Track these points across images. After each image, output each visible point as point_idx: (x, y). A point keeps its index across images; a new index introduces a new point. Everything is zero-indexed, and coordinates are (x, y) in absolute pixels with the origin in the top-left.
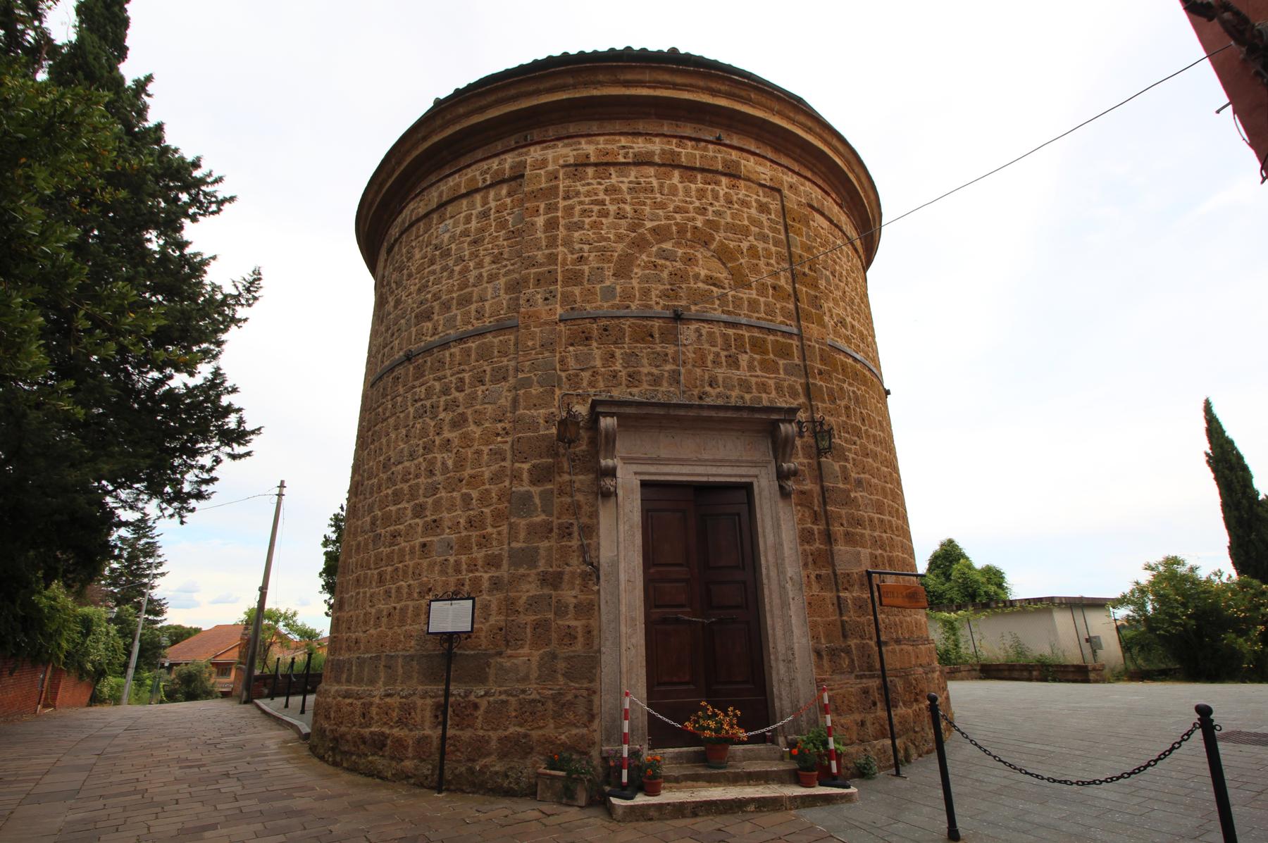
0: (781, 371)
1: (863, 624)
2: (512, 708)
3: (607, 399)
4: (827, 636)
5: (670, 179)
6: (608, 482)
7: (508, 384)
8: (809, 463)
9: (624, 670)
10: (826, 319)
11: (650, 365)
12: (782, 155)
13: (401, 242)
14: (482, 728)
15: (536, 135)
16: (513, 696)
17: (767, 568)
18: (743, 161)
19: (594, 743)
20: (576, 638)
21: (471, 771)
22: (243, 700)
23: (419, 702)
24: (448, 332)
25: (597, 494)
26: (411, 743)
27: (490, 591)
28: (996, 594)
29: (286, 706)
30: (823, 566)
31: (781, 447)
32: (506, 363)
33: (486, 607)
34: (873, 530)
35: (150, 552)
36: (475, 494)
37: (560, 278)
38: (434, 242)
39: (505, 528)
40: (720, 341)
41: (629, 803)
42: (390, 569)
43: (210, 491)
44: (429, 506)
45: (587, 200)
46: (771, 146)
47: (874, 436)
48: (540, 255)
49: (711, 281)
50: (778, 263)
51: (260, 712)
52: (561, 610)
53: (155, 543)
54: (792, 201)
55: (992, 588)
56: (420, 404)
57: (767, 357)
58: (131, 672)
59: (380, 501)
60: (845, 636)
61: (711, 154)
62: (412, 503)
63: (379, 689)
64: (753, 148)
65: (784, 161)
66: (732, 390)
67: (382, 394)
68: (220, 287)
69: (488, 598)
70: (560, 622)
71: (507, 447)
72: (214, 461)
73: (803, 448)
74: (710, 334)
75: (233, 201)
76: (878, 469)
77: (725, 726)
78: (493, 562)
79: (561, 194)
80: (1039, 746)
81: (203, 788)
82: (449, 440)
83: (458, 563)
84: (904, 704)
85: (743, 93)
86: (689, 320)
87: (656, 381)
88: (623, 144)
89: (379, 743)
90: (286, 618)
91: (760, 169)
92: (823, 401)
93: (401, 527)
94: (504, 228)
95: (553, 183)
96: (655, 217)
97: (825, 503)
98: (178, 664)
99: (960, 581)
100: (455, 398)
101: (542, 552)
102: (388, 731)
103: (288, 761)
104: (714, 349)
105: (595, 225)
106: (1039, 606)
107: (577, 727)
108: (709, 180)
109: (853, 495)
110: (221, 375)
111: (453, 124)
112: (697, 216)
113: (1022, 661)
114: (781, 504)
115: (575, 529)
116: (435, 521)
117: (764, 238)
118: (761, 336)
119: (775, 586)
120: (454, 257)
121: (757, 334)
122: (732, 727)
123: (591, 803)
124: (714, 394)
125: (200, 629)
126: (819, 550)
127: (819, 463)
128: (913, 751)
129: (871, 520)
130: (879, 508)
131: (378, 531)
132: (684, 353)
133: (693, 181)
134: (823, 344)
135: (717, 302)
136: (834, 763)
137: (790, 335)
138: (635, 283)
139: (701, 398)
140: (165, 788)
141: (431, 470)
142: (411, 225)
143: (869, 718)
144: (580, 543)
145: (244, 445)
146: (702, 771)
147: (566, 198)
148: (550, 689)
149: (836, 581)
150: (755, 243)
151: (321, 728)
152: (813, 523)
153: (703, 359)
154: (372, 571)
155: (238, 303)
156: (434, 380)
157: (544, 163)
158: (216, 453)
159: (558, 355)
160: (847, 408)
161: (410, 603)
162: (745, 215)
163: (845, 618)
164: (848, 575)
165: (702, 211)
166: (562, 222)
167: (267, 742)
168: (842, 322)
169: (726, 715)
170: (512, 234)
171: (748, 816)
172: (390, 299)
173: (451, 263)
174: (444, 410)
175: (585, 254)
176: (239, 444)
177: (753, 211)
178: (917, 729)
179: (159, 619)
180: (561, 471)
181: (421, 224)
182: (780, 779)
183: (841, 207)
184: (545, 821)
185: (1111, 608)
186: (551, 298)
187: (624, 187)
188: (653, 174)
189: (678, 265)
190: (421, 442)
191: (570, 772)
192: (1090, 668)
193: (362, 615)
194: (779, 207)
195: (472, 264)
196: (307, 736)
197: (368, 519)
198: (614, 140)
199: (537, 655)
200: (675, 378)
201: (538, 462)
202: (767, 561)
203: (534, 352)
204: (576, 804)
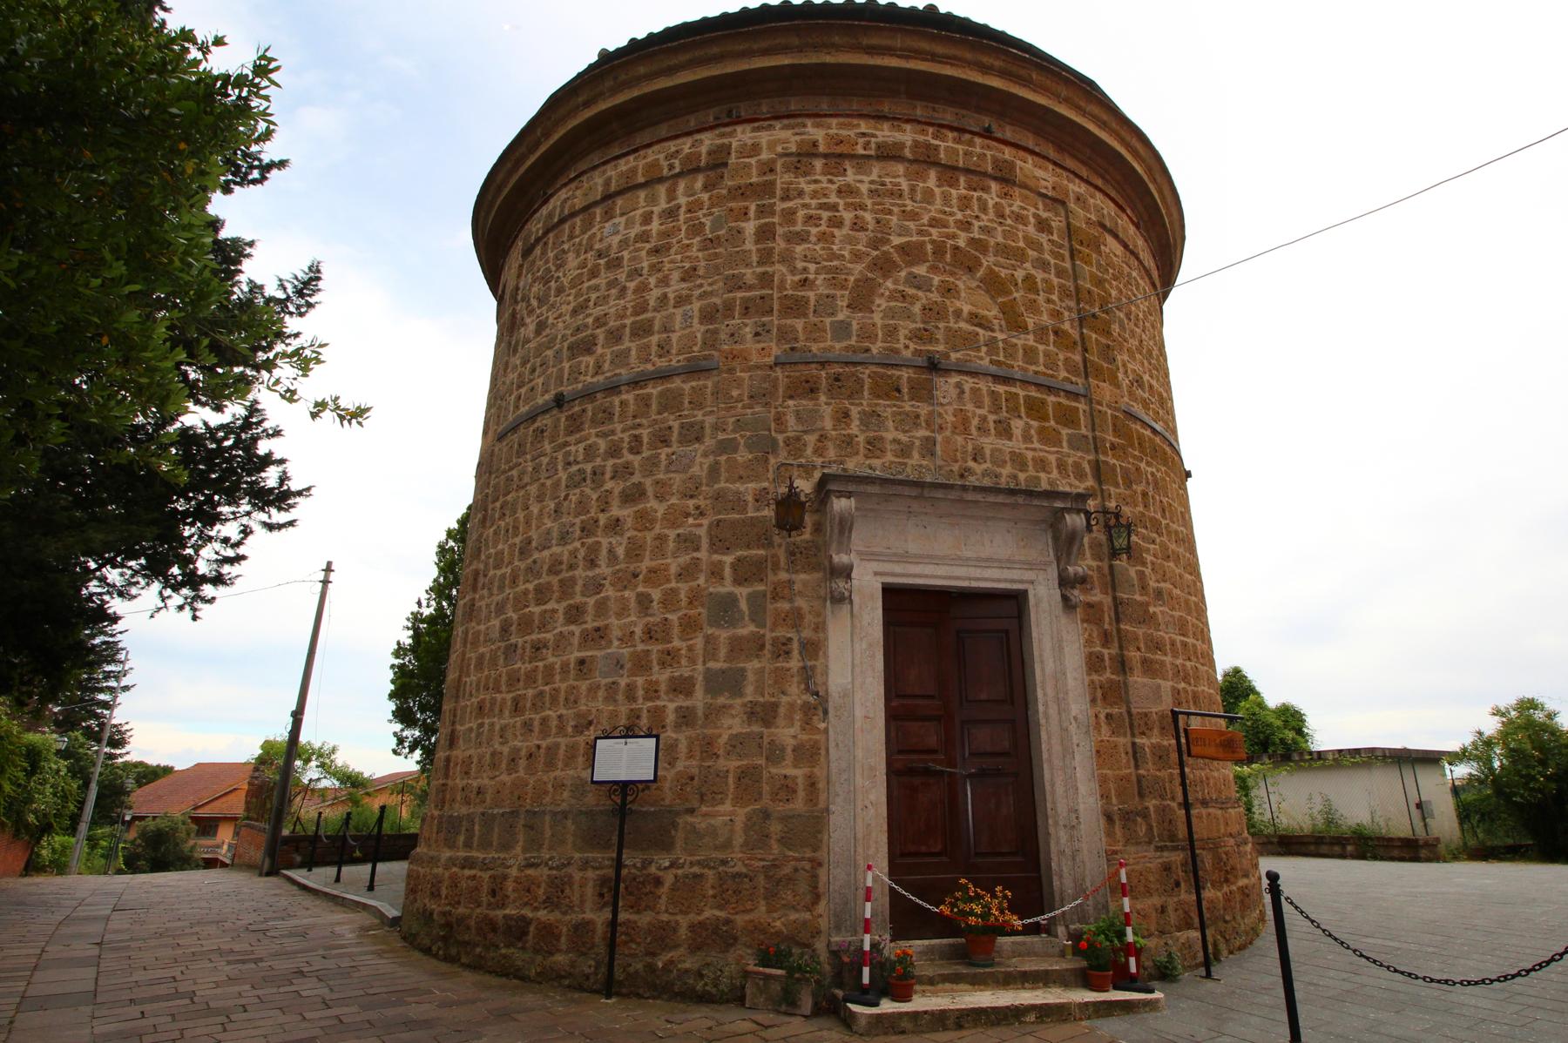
0: (1065, 444)
1: (1163, 780)
2: (709, 885)
3: (840, 472)
4: (1119, 795)
5: (925, 181)
6: (841, 584)
7: (703, 448)
8: (1099, 567)
9: (860, 835)
10: (1120, 376)
11: (896, 429)
12: (1066, 156)
13: (545, 244)
14: (666, 911)
15: (744, 110)
16: (710, 868)
17: (1046, 705)
18: (1018, 162)
19: (819, 932)
20: (795, 792)
21: (651, 968)
22: (265, 870)
23: (577, 876)
24: (617, 371)
25: (825, 600)
26: (565, 929)
27: (677, 727)
28: (1295, 742)
29: (338, 880)
30: (1116, 703)
31: (1065, 545)
32: (700, 418)
33: (673, 746)
34: (1175, 656)
35: (108, 656)
36: (656, 594)
37: (776, 307)
38: (597, 246)
39: (699, 642)
40: (987, 400)
41: (874, 1010)
42: (530, 692)
43: (233, 575)
44: (590, 609)
45: (814, 202)
46: (1052, 142)
47: (1176, 532)
48: (749, 275)
49: (975, 319)
50: (1061, 300)
51: (295, 888)
52: (775, 753)
53: (116, 643)
54: (1080, 217)
55: (1290, 735)
56: (574, 468)
57: (1047, 424)
58: (83, 827)
59: (515, 598)
60: (1141, 795)
61: (978, 150)
62: (564, 604)
63: (517, 855)
64: (1031, 145)
65: (1070, 163)
66: (1003, 467)
67: (518, 452)
68: (261, 287)
69: (674, 735)
70: (774, 771)
71: (702, 532)
72: (241, 532)
73: (1090, 547)
74: (975, 391)
75: (284, 166)
76: (1181, 576)
77: (994, 911)
78: (681, 687)
79: (778, 192)
80: (1380, 941)
81: (275, 990)
82: (618, 520)
83: (631, 688)
84: (1213, 886)
85: (1023, 72)
86: (947, 372)
87: (905, 451)
88: (863, 130)
89: (517, 930)
90: (320, 755)
91: (1040, 173)
92: (1117, 485)
93: (549, 636)
94: (698, 234)
95: (768, 177)
96: (904, 231)
97: (1118, 620)
98: (142, 818)
99: (1249, 723)
100: (627, 463)
101: (751, 677)
102: (530, 915)
103: (380, 954)
104: (979, 411)
105: (823, 237)
106: (1358, 759)
107: (797, 911)
108: (975, 185)
109: (1152, 609)
110: (258, 410)
111: (630, 88)
112: (959, 232)
113: (1333, 832)
114: (1064, 620)
115: (795, 645)
116: (597, 629)
117: (1043, 265)
118: (1039, 395)
119: (1054, 727)
120: (626, 269)
121: (1034, 393)
122: (1002, 912)
123: (818, 1012)
124: (979, 472)
125: (172, 768)
126: (1111, 681)
127: (1111, 567)
128: (1222, 946)
129: (1173, 644)
130: (1182, 628)
131: (513, 641)
132: (940, 415)
133: (953, 183)
134: (1116, 409)
135: (984, 349)
136: (1132, 960)
137: (1075, 396)
138: (877, 318)
139: (962, 476)
140: (219, 991)
141: (592, 560)
142: (562, 221)
143: (1171, 902)
144: (801, 664)
145: (286, 510)
146: (964, 970)
147: (786, 198)
148: (761, 860)
149: (1134, 723)
150: (1033, 272)
151: (425, 911)
152: (1103, 646)
153: (965, 422)
154: (504, 695)
155: (285, 310)
156: (597, 436)
157: (755, 149)
158: (245, 520)
159: (773, 411)
160: (1145, 494)
161: (562, 741)
162: (1020, 234)
163: (1141, 772)
164: (1146, 715)
165: (965, 225)
166: (780, 231)
167: (337, 929)
168: (1139, 381)
169: (994, 896)
170: (710, 243)
171: (1029, 1028)
172: (528, 320)
173: (622, 277)
174: (612, 478)
175: (811, 277)
176: (280, 509)
177: (1031, 229)
178: (1227, 918)
179: (118, 752)
180: (776, 567)
181: (578, 220)
182: (1062, 979)
183: (1137, 226)
184: (763, 1034)
185: (1447, 766)
186: (764, 333)
187: (864, 188)
188: (901, 173)
189: (935, 296)
190: (578, 521)
191: (791, 971)
192: (1421, 843)
193: (488, 756)
194: (1064, 224)
195: (652, 281)
196: (395, 922)
197: (496, 623)
198: (850, 124)
199: (741, 814)
200: (929, 447)
201: (745, 553)
202: (1045, 695)
203: (740, 405)
204: (798, 1012)
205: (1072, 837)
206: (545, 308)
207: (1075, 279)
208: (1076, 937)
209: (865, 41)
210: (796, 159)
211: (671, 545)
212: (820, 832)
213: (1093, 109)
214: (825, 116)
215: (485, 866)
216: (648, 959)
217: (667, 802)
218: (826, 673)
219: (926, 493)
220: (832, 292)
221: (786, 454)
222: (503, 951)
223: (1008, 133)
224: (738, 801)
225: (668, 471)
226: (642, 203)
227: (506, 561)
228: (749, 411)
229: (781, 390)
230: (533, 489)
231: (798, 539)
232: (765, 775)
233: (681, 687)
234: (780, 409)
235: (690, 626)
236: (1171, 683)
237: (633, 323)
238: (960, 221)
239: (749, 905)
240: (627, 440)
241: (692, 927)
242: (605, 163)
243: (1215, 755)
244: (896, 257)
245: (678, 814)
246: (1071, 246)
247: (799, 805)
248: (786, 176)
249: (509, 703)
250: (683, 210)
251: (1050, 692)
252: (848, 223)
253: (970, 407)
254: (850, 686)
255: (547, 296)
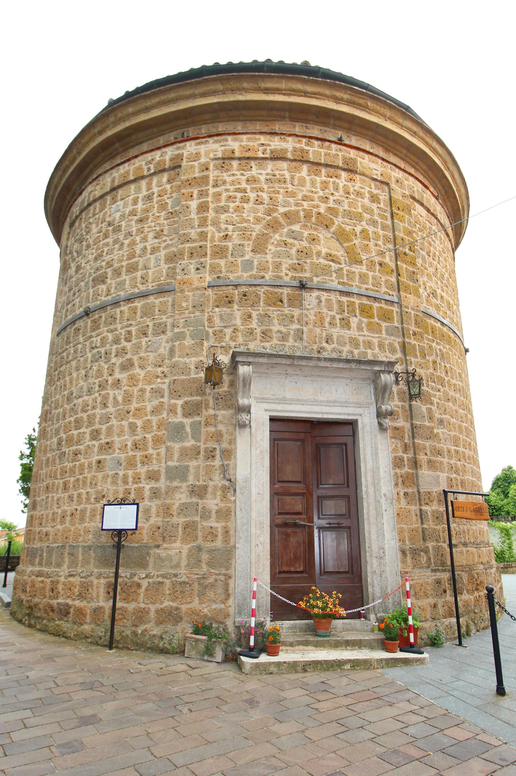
0: (384, 332)
1: (439, 531)
2: (167, 588)
3: (245, 351)
4: (411, 539)
5: (300, 173)
6: (244, 417)
7: (166, 337)
8: (402, 406)
9: (253, 561)
10: (421, 290)
11: (280, 324)
12: (391, 155)
13: (81, 219)
14: (143, 602)
15: (191, 132)
17: (367, 486)
18: (359, 159)
20: (216, 536)
21: (135, 634)
23: (95, 581)
24: (119, 293)
25: (235, 426)
27: (151, 499)
32: (164, 319)
33: (147, 511)
37: (209, 252)
38: (108, 219)
40: (335, 307)
42: (72, 479)
44: (104, 431)
45: (232, 188)
46: (382, 146)
47: (455, 385)
48: (193, 233)
49: (330, 257)
52: (206, 515)
54: (398, 193)
56: (96, 351)
57: (372, 320)
59: (65, 426)
60: (424, 539)
61: (334, 152)
62: (90, 429)
64: (368, 148)
65: (393, 159)
66: (344, 346)
67: (66, 342)
69: (149, 504)
70: (205, 524)
71: (165, 387)
74: (328, 301)
77: (330, 606)
78: (153, 476)
79: (211, 182)
82: (119, 380)
83: (125, 477)
84: (468, 592)
85: (362, 102)
87: (284, 338)
88: (262, 142)
91: (373, 166)
92: (416, 356)
93: (81, 447)
94: (164, 210)
97: (413, 437)
100: (124, 347)
101: (192, 470)
104: (330, 313)
105: (237, 209)
107: (216, 603)
108: (331, 174)
109: (435, 431)
111: (124, 121)
112: (321, 204)
114: (379, 437)
115: (218, 452)
116: (108, 443)
117: (374, 223)
118: (368, 303)
119: (372, 500)
122: (335, 606)
123: (226, 660)
126: (408, 473)
127: (410, 406)
128: (472, 627)
130: (456, 441)
131: (63, 450)
132: (306, 316)
133: (317, 173)
135: (334, 275)
136: (412, 635)
138: (269, 257)
141: (105, 404)
142: (89, 205)
143: (440, 602)
144: (221, 463)
146: (311, 638)
147: (215, 186)
148: (196, 574)
150: (367, 227)
153: (322, 320)
154: (59, 481)
156: (108, 332)
157: (198, 156)
159: (206, 315)
161: (89, 507)
162: (360, 204)
163: (425, 526)
166: (211, 206)
168: (434, 294)
171: (345, 673)
172: (72, 265)
173: (121, 237)
177: (366, 201)
178: (476, 611)
180: (207, 407)
181: (97, 204)
182: (370, 645)
183: (437, 198)
187: (262, 178)
188: (286, 168)
189: (305, 244)
190: (97, 381)
191: (210, 637)
193: (51, 515)
194: (387, 198)
195: (138, 239)
196: (8, 605)
197: (55, 440)
199: (186, 549)
200: (299, 335)
201: (190, 399)
202: (367, 481)
203: (187, 312)
205: (380, 563)
206: (80, 257)
207: (394, 232)
208: (381, 620)
209: (263, 85)
210: (222, 161)
211: (148, 394)
212: (230, 559)
213: (408, 124)
214: (239, 134)
215: (48, 576)
216: (134, 629)
217: (145, 541)
218: (235, 468)
219: (296, 362)
220: (242, 242)
221: (214, 340)
222: (57, 622)
223: (354, 141)
224: (184, 541)
225: (147, 351)
226: (133, 192)
227: (60, 404)
228: (192, 315)
229: (211, 302)
230: (74, 363)
231: (220, 390)
232: (200, 526)
233: (153, 476)
234: (211, 314)
235: (158, 441)
236: (447, 474)
237: (128, 264)
238: (322, 197)
239: (189, 600)
240: (123, 333)
241: (157, 611)
242: (112, 169)
243: (470, 517)
244: (281, 220)
245: (150, 548)
246: (392, 211)
247: (219, 543)
248: (216, 172)
249: (61, 485)
250: (155, 195)
251: (370, 479)
252: (252, 200)
253: (325, 310)
254: (249, 476)
255: (81, 250)
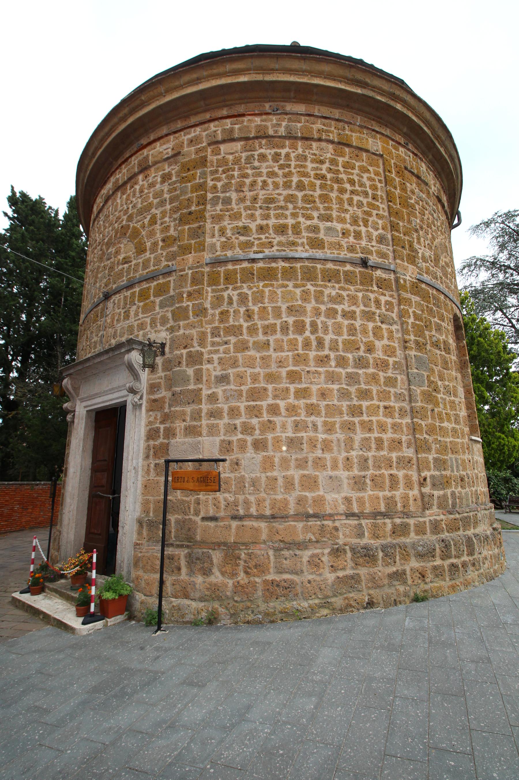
85: (138, 102)
